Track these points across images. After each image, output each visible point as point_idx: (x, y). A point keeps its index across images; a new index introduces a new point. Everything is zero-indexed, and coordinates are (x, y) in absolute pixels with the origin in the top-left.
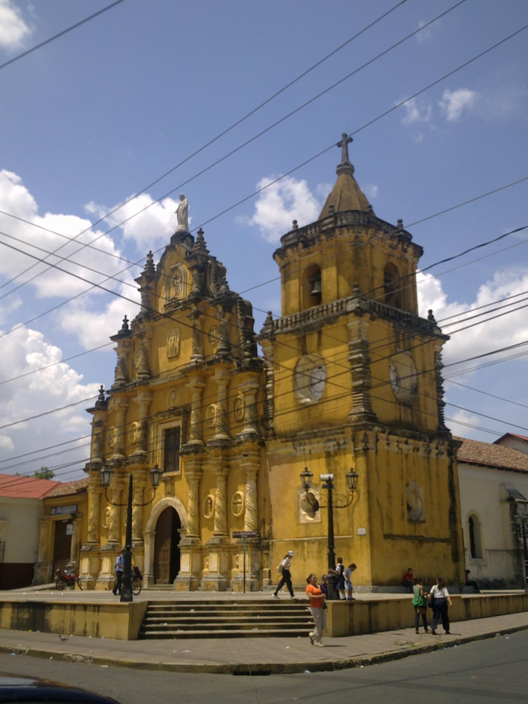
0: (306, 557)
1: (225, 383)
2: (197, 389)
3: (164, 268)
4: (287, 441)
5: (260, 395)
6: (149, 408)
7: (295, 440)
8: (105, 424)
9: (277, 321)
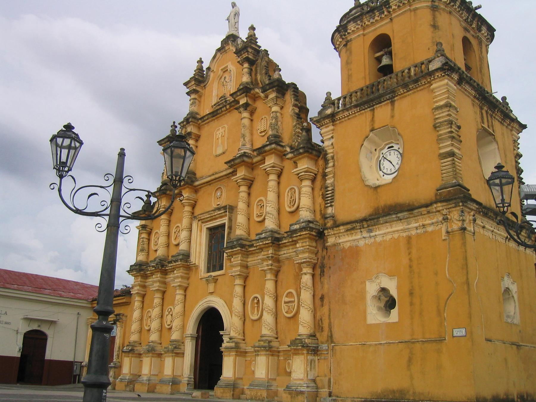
9: (339, 99)
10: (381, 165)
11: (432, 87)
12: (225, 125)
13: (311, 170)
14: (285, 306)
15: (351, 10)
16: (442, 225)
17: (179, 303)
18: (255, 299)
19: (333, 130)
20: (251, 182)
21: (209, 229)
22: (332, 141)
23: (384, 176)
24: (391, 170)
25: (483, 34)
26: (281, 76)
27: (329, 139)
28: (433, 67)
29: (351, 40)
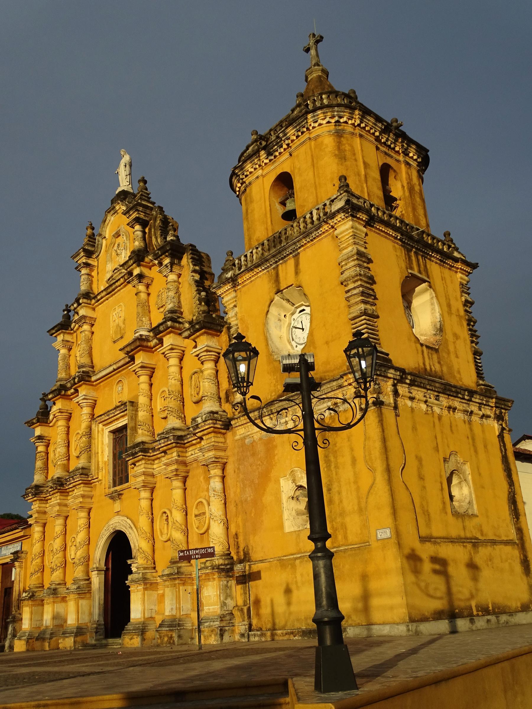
3: (105, 237)
11: (336, 232)
13: (211, 349)
19: (236, 297)
21: (114, 432)
22: (236, 309)
23: (297, 347)
25: (412, 158)
29: (250, 183)
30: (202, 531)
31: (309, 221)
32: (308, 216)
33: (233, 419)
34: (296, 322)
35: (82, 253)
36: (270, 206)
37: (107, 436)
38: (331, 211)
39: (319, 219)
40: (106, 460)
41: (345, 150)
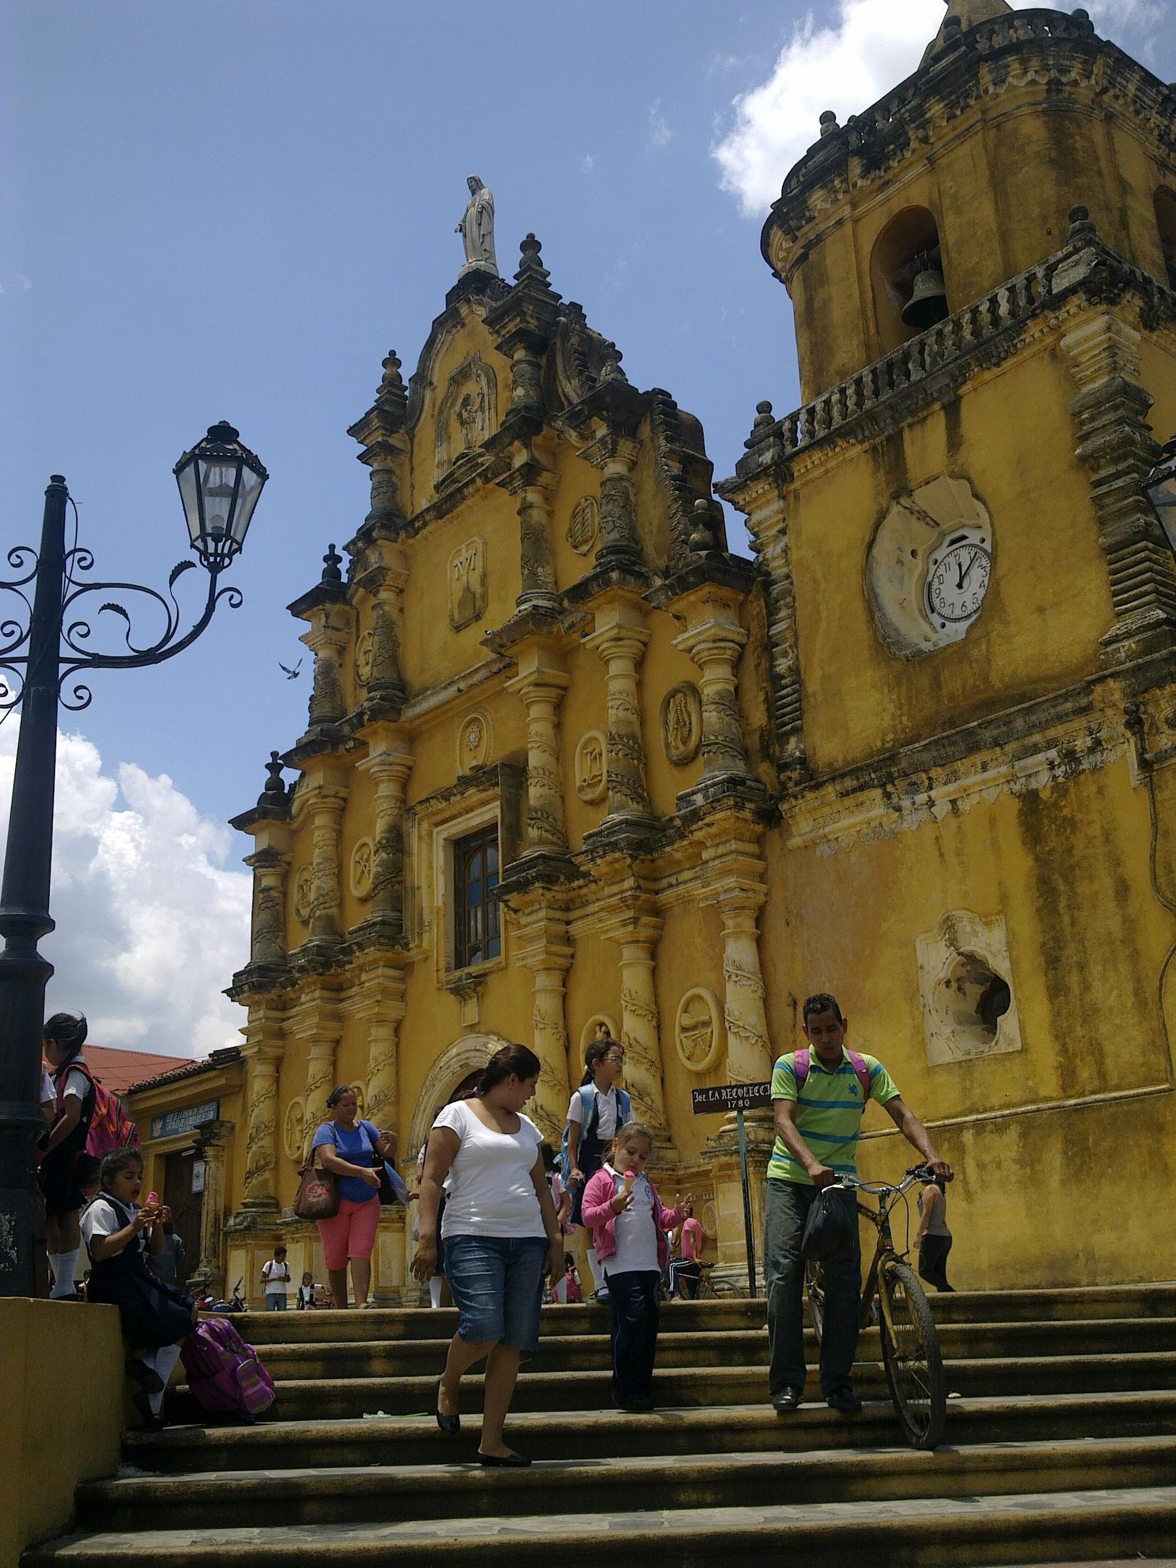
0: (973, 1187)
1: (630, 648)
2: (542, 692)
3: (431, 383)
4: (862, 788)
5: (750, 661)
6: (405, 783)
7: (891, 779)
8: (286, 858)
9: (794, 418)
10: (934, 595)
12: (474, 538)
14: (684, 1040)
15: (813, 151)
16: (1127, 743)
17: (380, 1067)
18: (598, 1028)
20: (561, 692)
22: (785, 539)
24: (963, 605)
26: (623, 374)
27: (776, 538)
28: (1060, 283)
29: (819, 239)
30: (701, 1066)
31: (986, 318)
32: (984, 308)
33: (782, 798)
34: (942, 567)
35: (376, 420)
36: (873, 290)
37: (441, 849)
38: (1050, 291)
39: (1012, 313)
40: (441, 904)
41: (1075, 149)
